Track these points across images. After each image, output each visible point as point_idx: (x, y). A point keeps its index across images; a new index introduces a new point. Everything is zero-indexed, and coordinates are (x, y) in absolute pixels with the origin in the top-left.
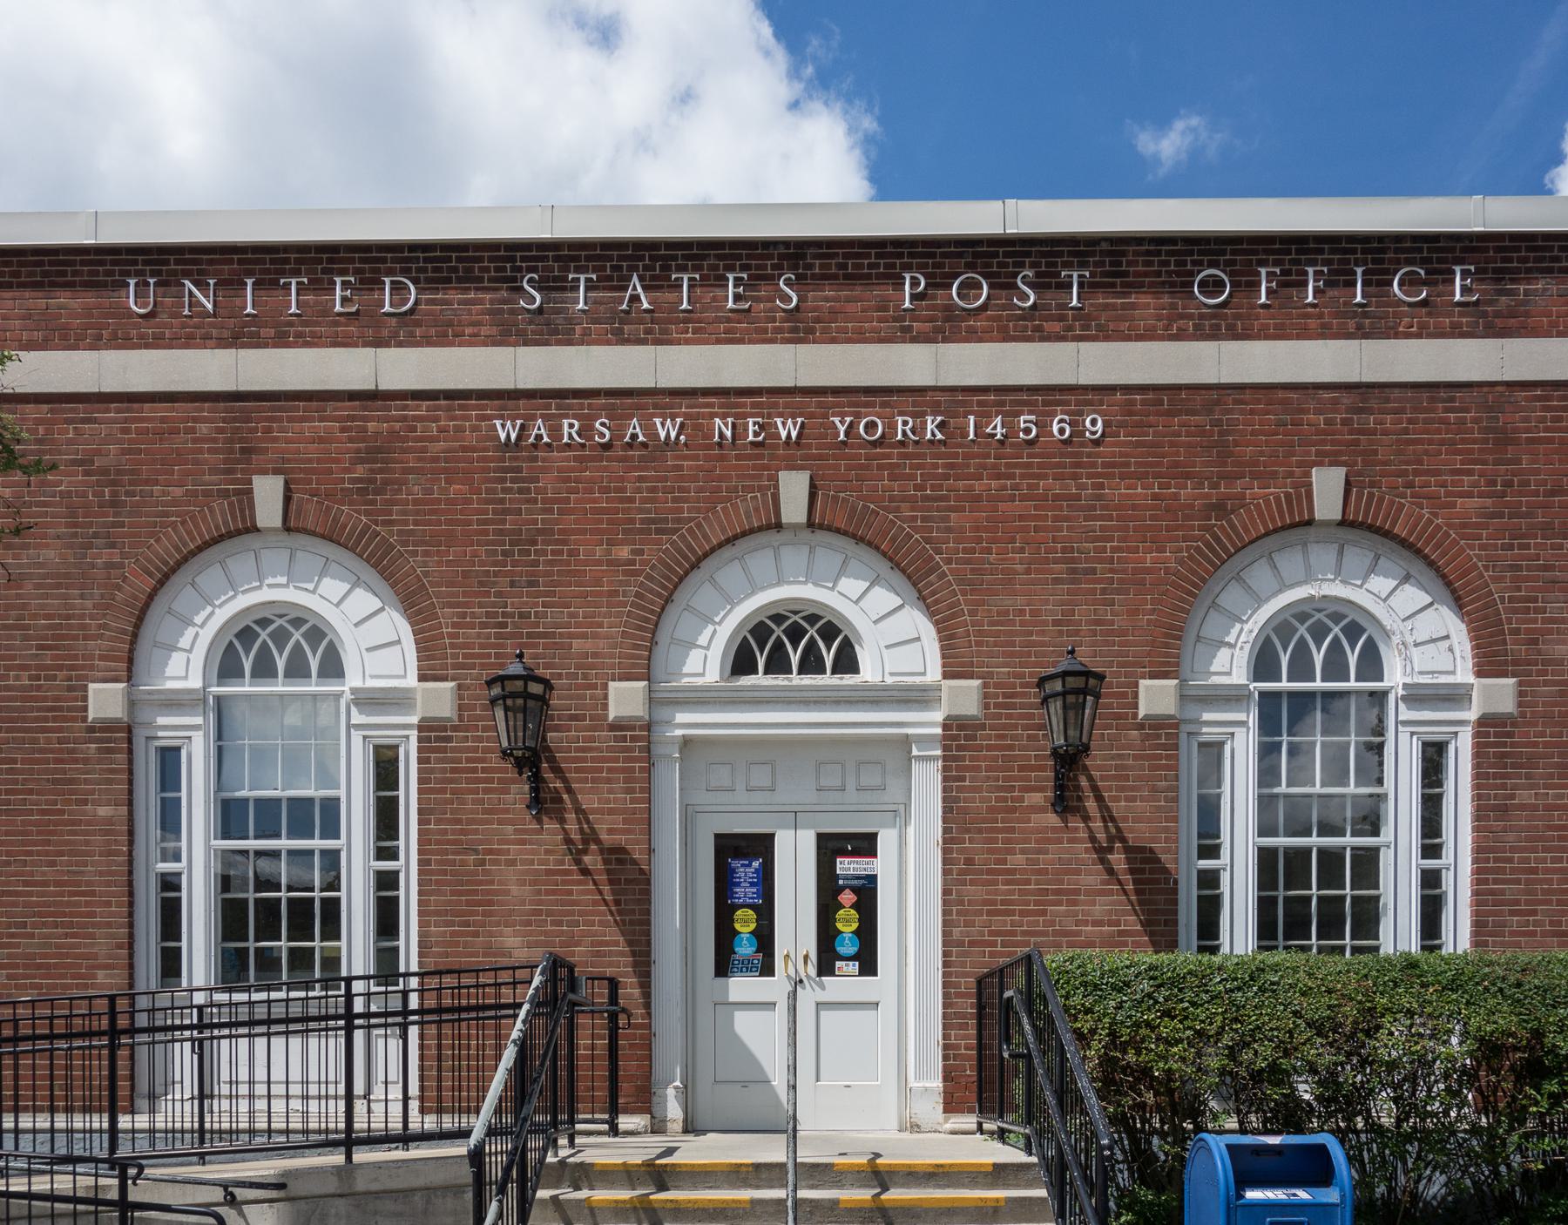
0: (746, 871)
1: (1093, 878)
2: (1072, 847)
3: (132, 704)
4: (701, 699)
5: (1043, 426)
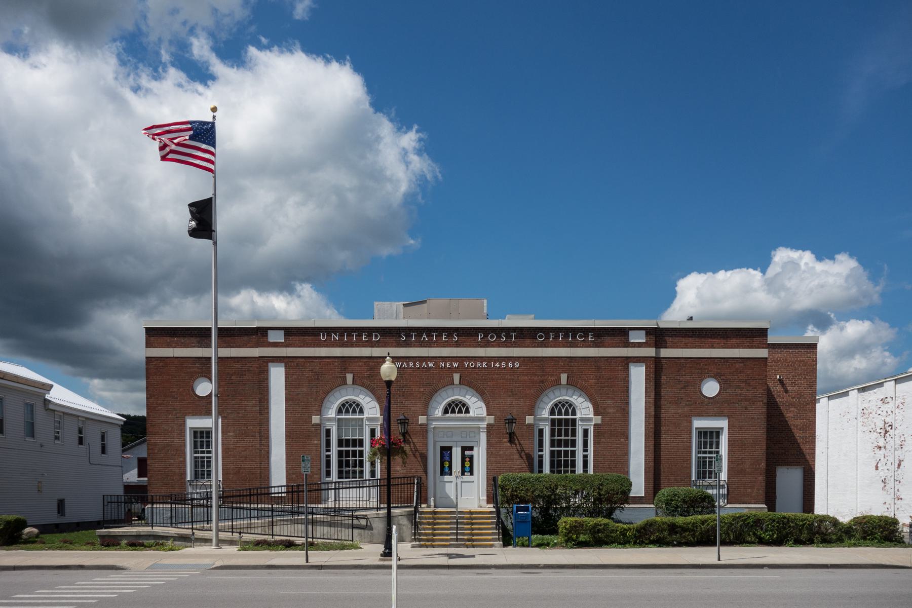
0: (447, 453)
1: (517, 456)
2: (513, 450)
3: (321, 420)
4: (438, 419)
5: (507, 365)
